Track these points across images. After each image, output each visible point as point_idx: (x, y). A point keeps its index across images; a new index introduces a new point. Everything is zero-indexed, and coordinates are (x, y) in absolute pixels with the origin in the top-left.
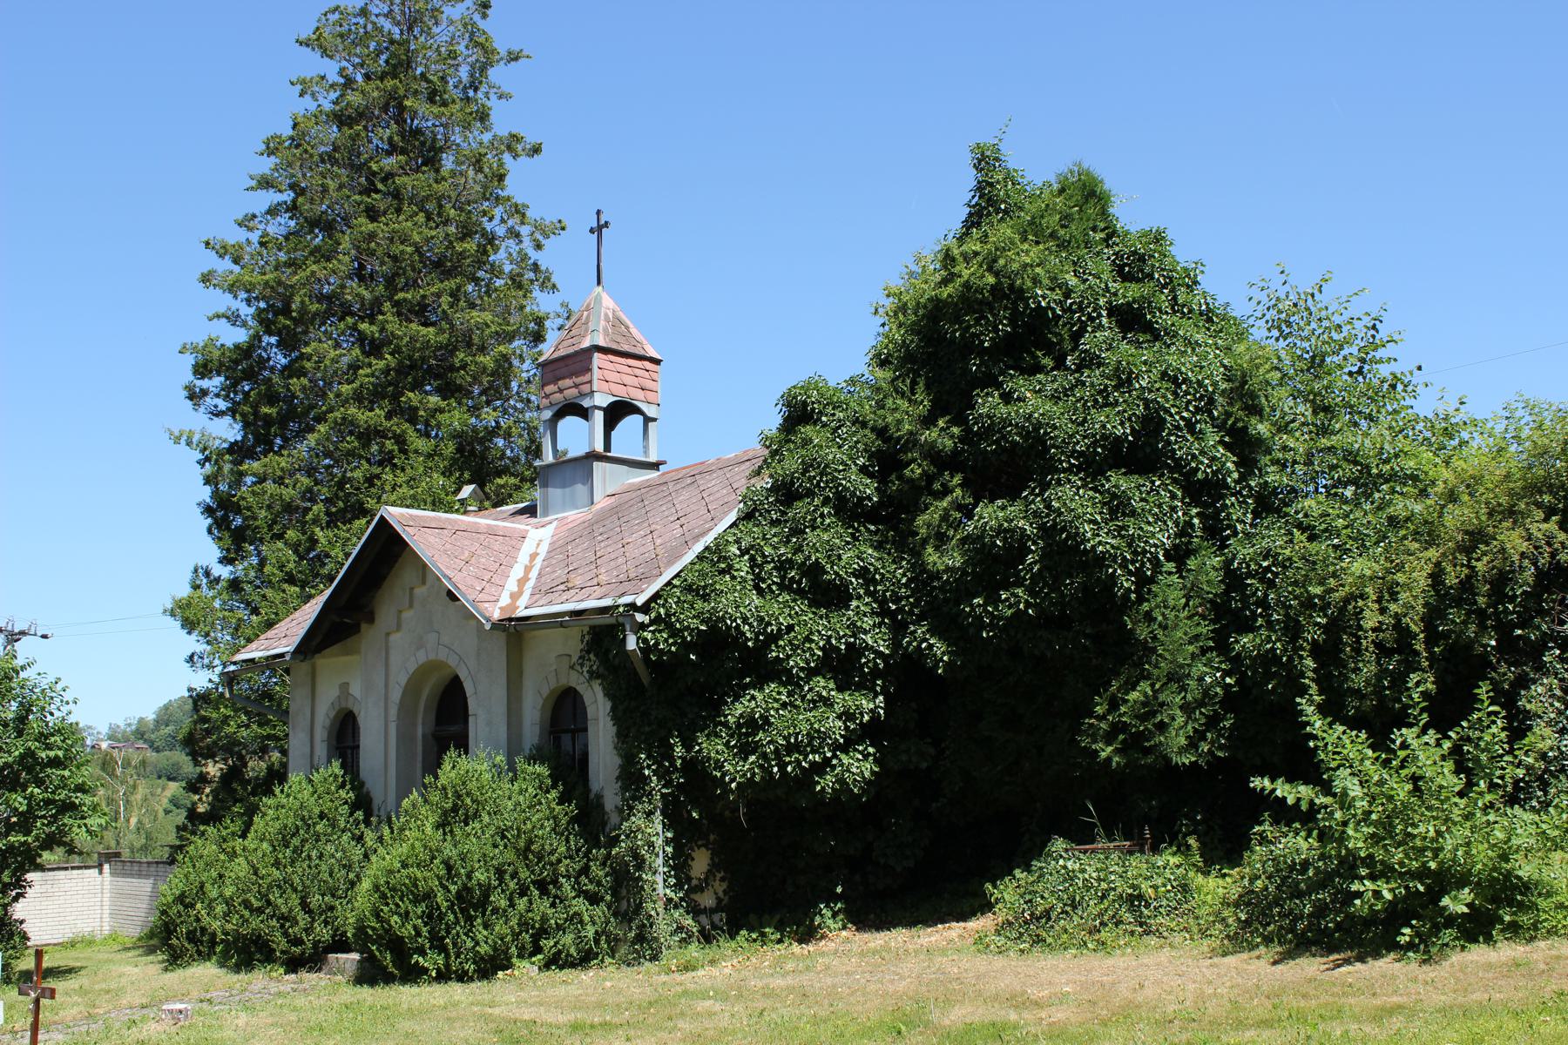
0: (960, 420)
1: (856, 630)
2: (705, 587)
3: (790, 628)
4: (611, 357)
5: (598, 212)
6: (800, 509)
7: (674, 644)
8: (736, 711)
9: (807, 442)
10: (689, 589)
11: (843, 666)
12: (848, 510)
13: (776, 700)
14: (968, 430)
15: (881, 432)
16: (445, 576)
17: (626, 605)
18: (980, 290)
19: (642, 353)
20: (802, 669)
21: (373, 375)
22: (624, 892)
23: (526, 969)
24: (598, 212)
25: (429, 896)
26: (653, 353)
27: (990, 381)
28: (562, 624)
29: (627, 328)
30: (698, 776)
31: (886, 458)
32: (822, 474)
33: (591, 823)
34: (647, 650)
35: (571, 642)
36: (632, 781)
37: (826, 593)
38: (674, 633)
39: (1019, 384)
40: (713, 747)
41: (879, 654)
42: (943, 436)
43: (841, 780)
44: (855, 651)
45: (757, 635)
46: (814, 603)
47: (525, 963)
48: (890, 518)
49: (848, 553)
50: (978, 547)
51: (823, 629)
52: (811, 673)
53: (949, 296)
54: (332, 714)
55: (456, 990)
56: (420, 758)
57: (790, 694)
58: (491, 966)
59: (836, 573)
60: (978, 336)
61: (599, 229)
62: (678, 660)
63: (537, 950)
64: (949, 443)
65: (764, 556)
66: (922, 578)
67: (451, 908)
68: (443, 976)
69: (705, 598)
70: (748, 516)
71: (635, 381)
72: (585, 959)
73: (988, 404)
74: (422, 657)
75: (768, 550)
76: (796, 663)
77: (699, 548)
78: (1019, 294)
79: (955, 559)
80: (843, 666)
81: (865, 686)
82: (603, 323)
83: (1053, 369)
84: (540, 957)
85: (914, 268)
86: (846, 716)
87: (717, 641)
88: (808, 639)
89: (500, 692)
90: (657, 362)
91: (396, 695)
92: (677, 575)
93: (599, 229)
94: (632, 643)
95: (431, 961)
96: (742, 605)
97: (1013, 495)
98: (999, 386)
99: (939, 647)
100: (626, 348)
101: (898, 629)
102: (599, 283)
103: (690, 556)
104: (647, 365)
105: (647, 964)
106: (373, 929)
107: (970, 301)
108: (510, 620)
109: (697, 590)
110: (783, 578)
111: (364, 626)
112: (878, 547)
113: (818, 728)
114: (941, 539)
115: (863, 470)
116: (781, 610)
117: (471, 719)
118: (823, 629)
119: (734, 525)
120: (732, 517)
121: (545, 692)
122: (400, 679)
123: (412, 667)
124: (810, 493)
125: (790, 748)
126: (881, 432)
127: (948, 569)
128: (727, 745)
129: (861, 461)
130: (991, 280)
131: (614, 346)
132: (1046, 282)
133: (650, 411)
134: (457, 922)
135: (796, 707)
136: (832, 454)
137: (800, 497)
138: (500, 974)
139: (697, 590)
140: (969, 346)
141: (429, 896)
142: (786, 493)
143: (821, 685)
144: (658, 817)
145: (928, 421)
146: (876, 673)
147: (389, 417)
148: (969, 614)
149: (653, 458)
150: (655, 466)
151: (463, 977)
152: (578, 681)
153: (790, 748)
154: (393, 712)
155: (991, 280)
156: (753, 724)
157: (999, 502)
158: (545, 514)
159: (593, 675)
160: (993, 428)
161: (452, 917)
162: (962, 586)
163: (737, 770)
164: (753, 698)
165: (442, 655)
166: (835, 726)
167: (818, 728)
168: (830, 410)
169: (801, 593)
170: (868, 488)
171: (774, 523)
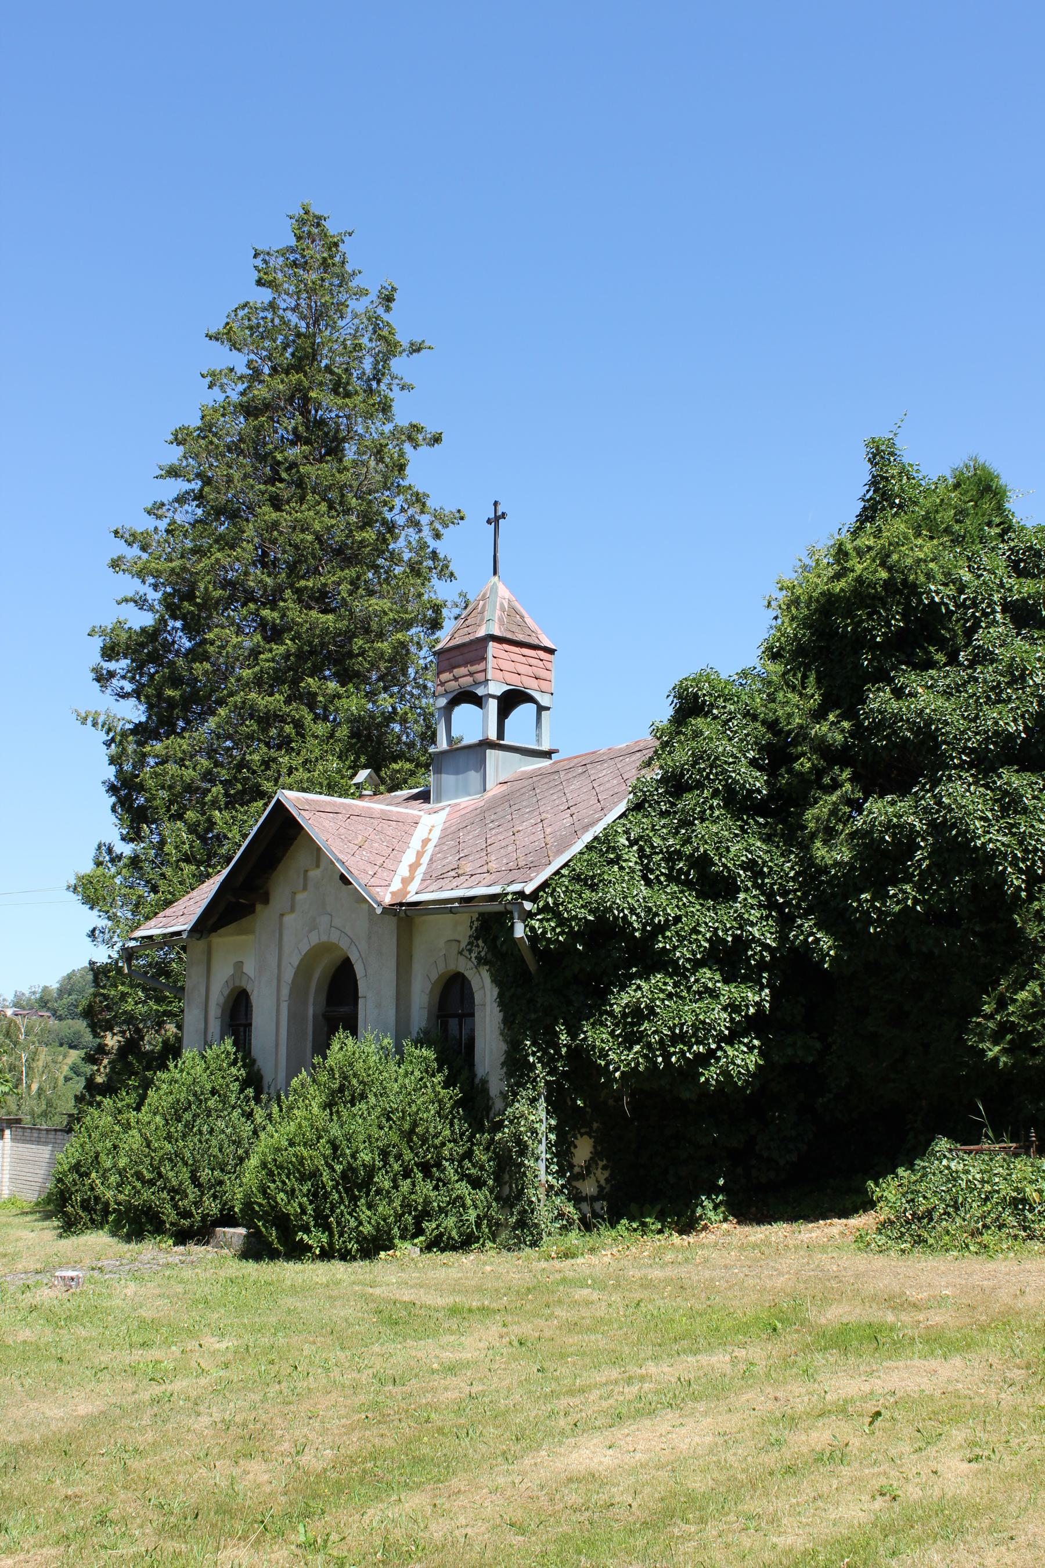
0: (850, 714)
1: (743, 922)
2: (593, 877)
3: (677, 919)
4: (506, 647)
5: (496, 504)
6: (689, 801)
7: (562, 933)
8: (622, 1000)
9: (697, 734)
10: (577, 878)
11: (729, 958)
12: (738, 803)
13: (662, 991)
14: (858, 725)
15: (772, 726)
16: (338, 860)
17: (514, 893)
18: (872, 585)
19: (536, 642)
20: (688, 960)
21: (273, 660)
22: (506, 1177)
23: (408, 1250)
24: (496, 504)
25: (315, 1174)
26: (547, 643)
27: (882, 676)
28: (451, 911)
29: (522, 617)
30: (582, 1060)
31: (776, 752)
32: (711, 767)
33: (475, 1107)
34: (534, 938)
35: (462, 928)
36: (517, 1067)
37: (715, 887)
38: (562, 922)
39: (910, 679)
40: (598, 1036)
41: (766, 947)
42: (832, 730)
43: (725, 1073)
44: (742, 943)
45: (644, 925)
46: (702, 895)
47: (407, 1244)
48: (779, 810)
49: (736, 845)
50: (866, 843)
51: (711, 920)
52: (697, 964)
53: (842, 590)
54: (226, 992)
55: (338, 1268)
56: (310, 1037)
57: (676, 985)
58: (373, 1246)
59: (724, 865)
60: (870, 631)
61: (496, 520)
62: (566, 949)
63: (420, 1232)
64: (839, 738)
65: (653, 847)
66: (810, 872)
67: (335, 1187)
68: (326, 1255)
69: (593, 888)
70: (637, 807)
71: (528, 670)
72: (466, 1243)
73: (879, 699)
74: (314, 939)
75: (657, 841)
76: (682, 954)
77: (588, 837)
78: (913, 589)
79: (844, 854)
80: (729, 958)
81: (752, 978)
82: (498, 612)
83: (945, 665)
84: (422, 1238)
85: (807, 561)
86: (732, 1007)
87: (604, 930)
88: (695, 931)
89: (389, 974)
90: (551, 651)
91: (289, 975)
92: (566, 865)
93: (496, 520)
94: (519, 931)
95: (315, 1239)
96: (630, 895)
97: (903, 790)
98: (890, 681)
99: (826, 942)
100: (520, 637)
101: (785, 922)
102: (495, 573)
103: (579, 846)
104: (542, 654)
105: (528, 1250)
106: (260, 1205)
107: (863, 596)
108: (401, 904)
109: (586, 880)
110: (671, 869)
111: (259, 907)
112: (767, 839)
113: (700, 1019)
114: (829, 834)
115: (753, 763)
116: (668, 901)
117: (361, 1001)
118: (711, 920)
119: (623, 815)
120: (622, 808)
121: (434, 977)
122: (293, 959)
123: (305, 948)
124: (700, 785)
125: (675, 1039)
126: (772, 726)
127: (836, 864)
128: (612, 1033)
129: (751, 755)
130: (884, 575)
131: (509, 636)
132: (940, 577)
133: (544, 700)
134: (342, 1202)
135: (682, 998)
136: (722, 746)
137: (689, 789)
138: (382, 1254)
139: (586, 880)
140: (860, 641)
141: (315, 1174)
142: (676, 784)
143: (707, 976)
144: (542, 1104)
145: (819, 715)
146: (762, 966)
147: (288, 701)
148: (856, 909)
149: (545, 747)
150: (547, 754)
151: (345, 1256)
152: (466, 967)
153: (675, 1039)
154: (285, 991)
155: (884, 575)
156: (638, 1014)
157: (889, 798)
158: (438, 800)
159: (481, 961)
160: (884, 724)
161: (336, 1197)
162: (851, 881)
163: (622, 1059)
164: (639, 988)
165: (334, 937)
166: (720, 1018)
167: (700, 1019)
168: (720, 702)
169: (688, 884)
170: (758, 781)
171: (663, 814)
